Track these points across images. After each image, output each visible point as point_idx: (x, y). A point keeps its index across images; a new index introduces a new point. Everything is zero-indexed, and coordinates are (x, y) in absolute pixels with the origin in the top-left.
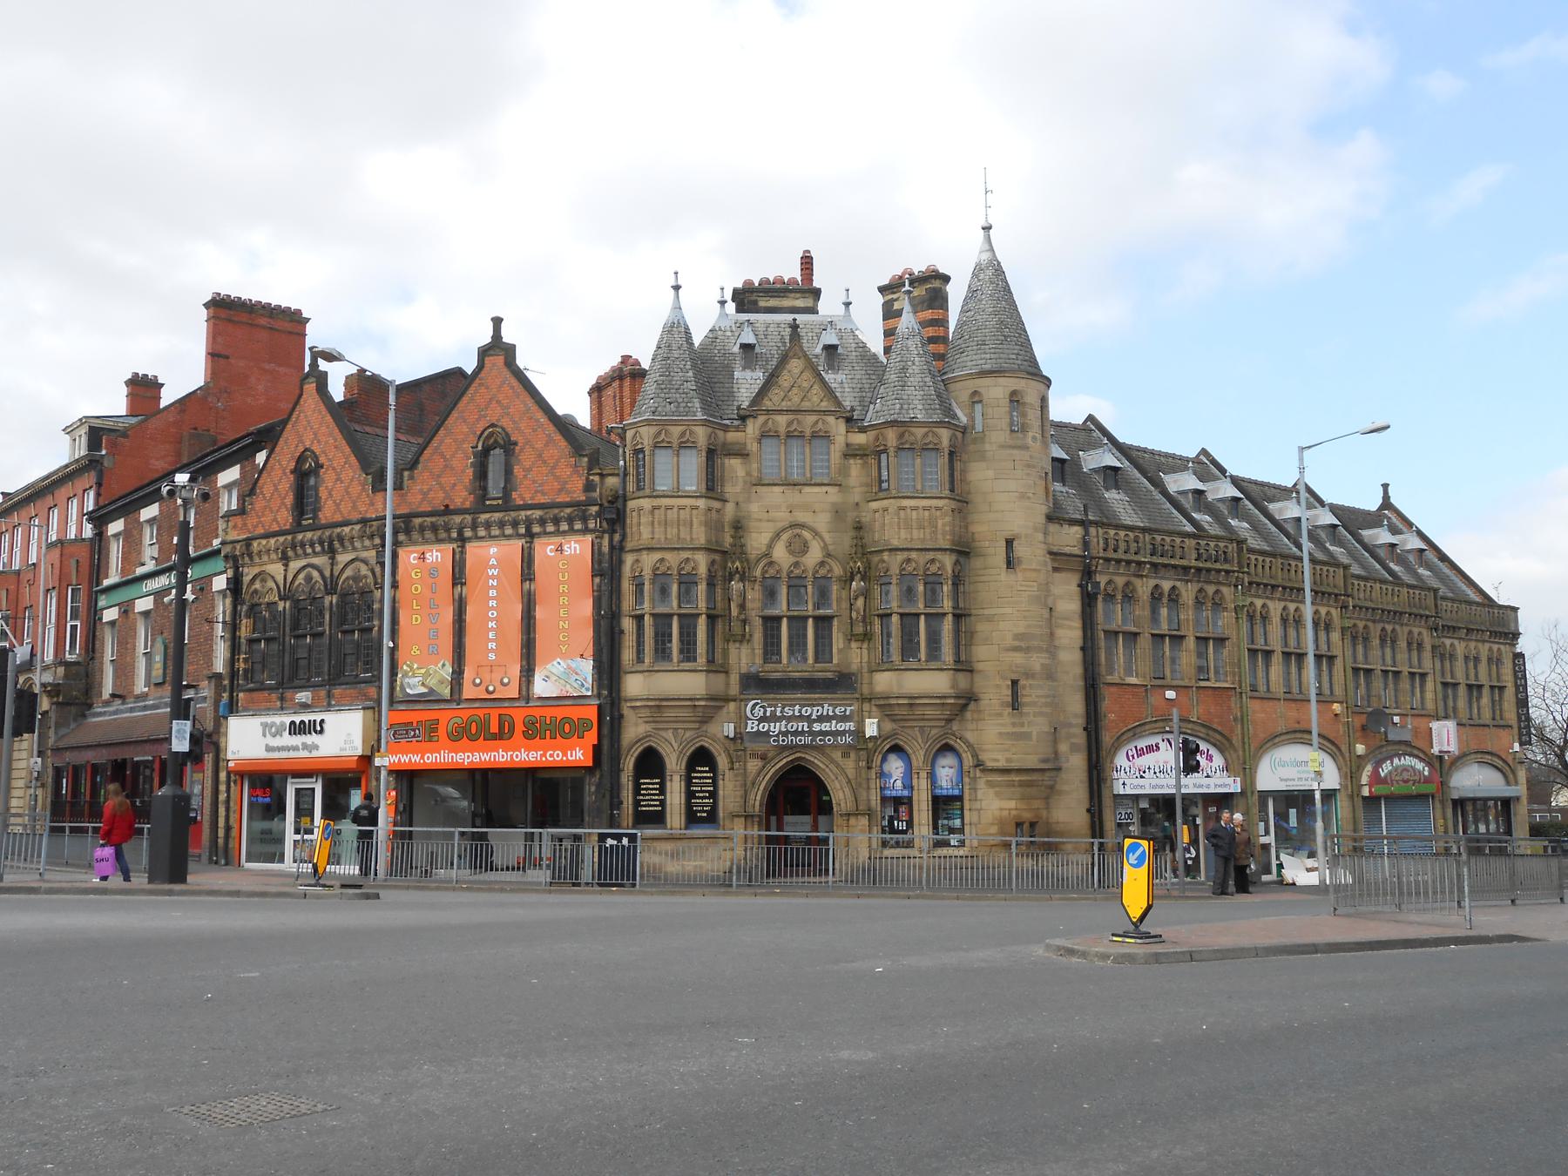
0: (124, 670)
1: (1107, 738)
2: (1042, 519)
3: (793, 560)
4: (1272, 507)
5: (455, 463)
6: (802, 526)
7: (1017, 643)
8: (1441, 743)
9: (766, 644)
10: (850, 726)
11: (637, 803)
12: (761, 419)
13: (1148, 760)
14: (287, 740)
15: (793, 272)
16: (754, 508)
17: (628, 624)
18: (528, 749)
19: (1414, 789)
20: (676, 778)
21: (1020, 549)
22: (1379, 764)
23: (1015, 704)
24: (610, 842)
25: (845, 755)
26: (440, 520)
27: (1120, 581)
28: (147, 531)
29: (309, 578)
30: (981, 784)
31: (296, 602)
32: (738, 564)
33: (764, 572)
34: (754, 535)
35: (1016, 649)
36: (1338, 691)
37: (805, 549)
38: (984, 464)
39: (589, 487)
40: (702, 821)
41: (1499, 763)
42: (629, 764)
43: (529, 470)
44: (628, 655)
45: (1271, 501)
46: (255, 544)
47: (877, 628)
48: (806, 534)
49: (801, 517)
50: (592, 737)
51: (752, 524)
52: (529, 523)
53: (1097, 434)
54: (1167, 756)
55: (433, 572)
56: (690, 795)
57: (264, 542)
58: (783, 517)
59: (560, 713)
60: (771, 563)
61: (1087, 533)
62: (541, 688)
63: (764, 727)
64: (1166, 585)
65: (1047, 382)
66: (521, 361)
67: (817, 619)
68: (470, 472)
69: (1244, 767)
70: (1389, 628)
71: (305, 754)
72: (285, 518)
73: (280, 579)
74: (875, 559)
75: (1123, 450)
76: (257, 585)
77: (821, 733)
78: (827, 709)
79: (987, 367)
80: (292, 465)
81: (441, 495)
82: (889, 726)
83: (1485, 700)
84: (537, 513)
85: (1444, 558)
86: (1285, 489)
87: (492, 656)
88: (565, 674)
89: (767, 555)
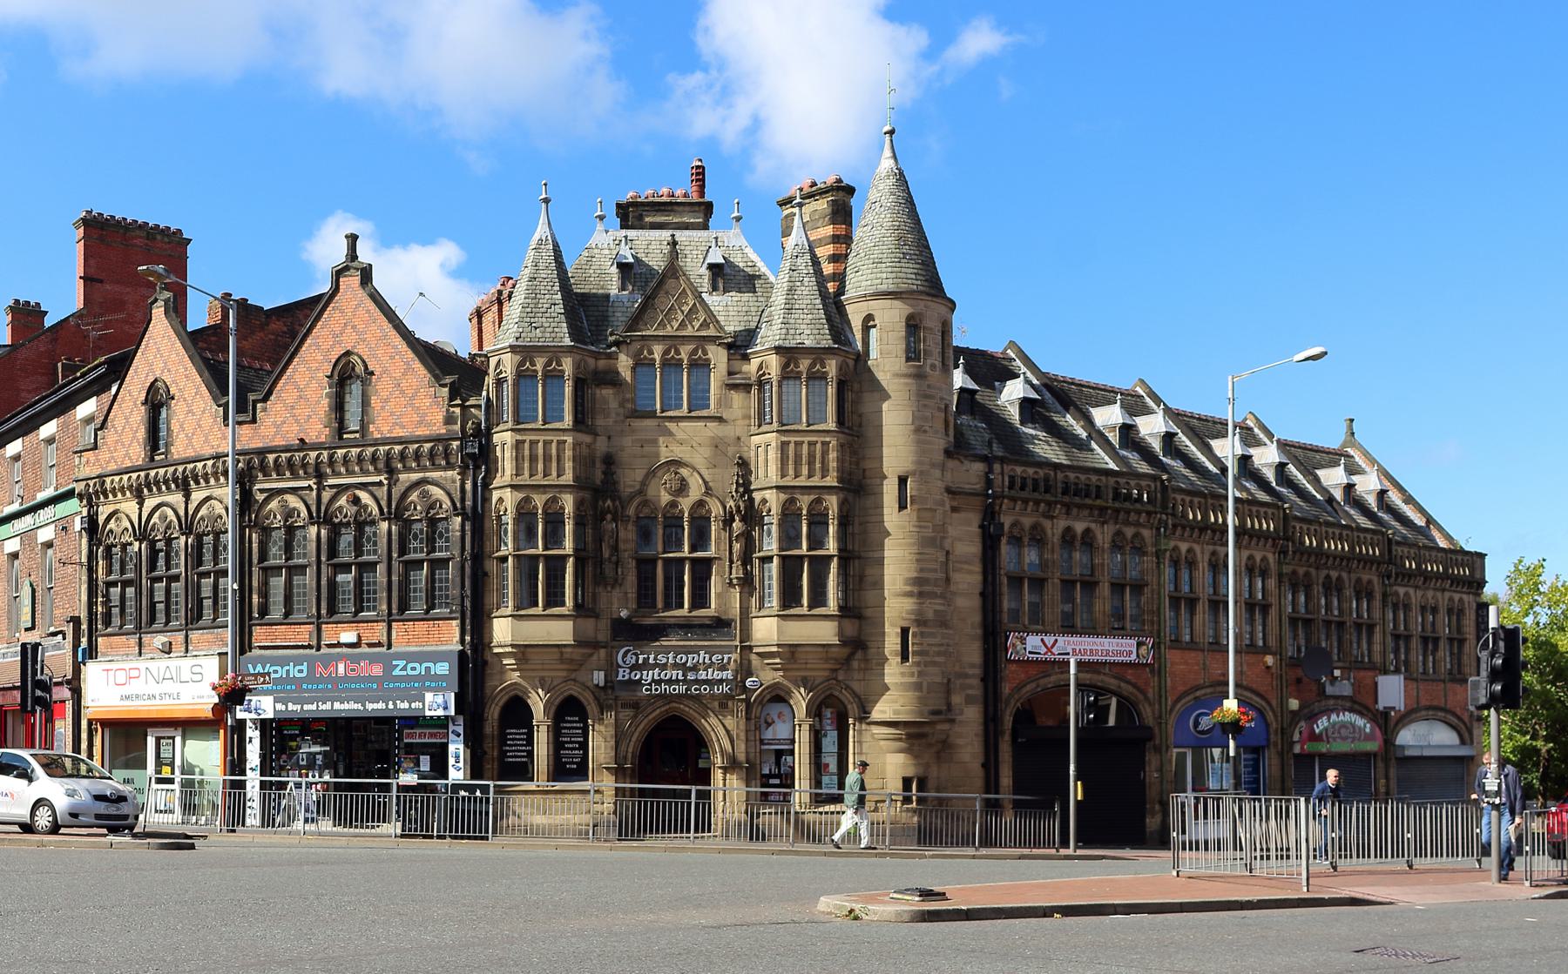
2: (939, 457)
7: (908, 588)
12: (637, 345)
15: (683, 188)
20: (543, 729)
26: (298, 456)
29: (164, 518)
30: (867, 737)
31: (152, 543)
39: (449, 420)
41: (1454, 720)
43: (386, 401)
48: (684, 472)
57: (117, 478)
60: (646, 503)
64: (1079, 527)
65: (952, 305)
67: (694, 561)
68: (325, 402)
72: (136, 453)
76: (112, 525)
79: (884, 288)
81: (295, 428)
89: (641, 492)
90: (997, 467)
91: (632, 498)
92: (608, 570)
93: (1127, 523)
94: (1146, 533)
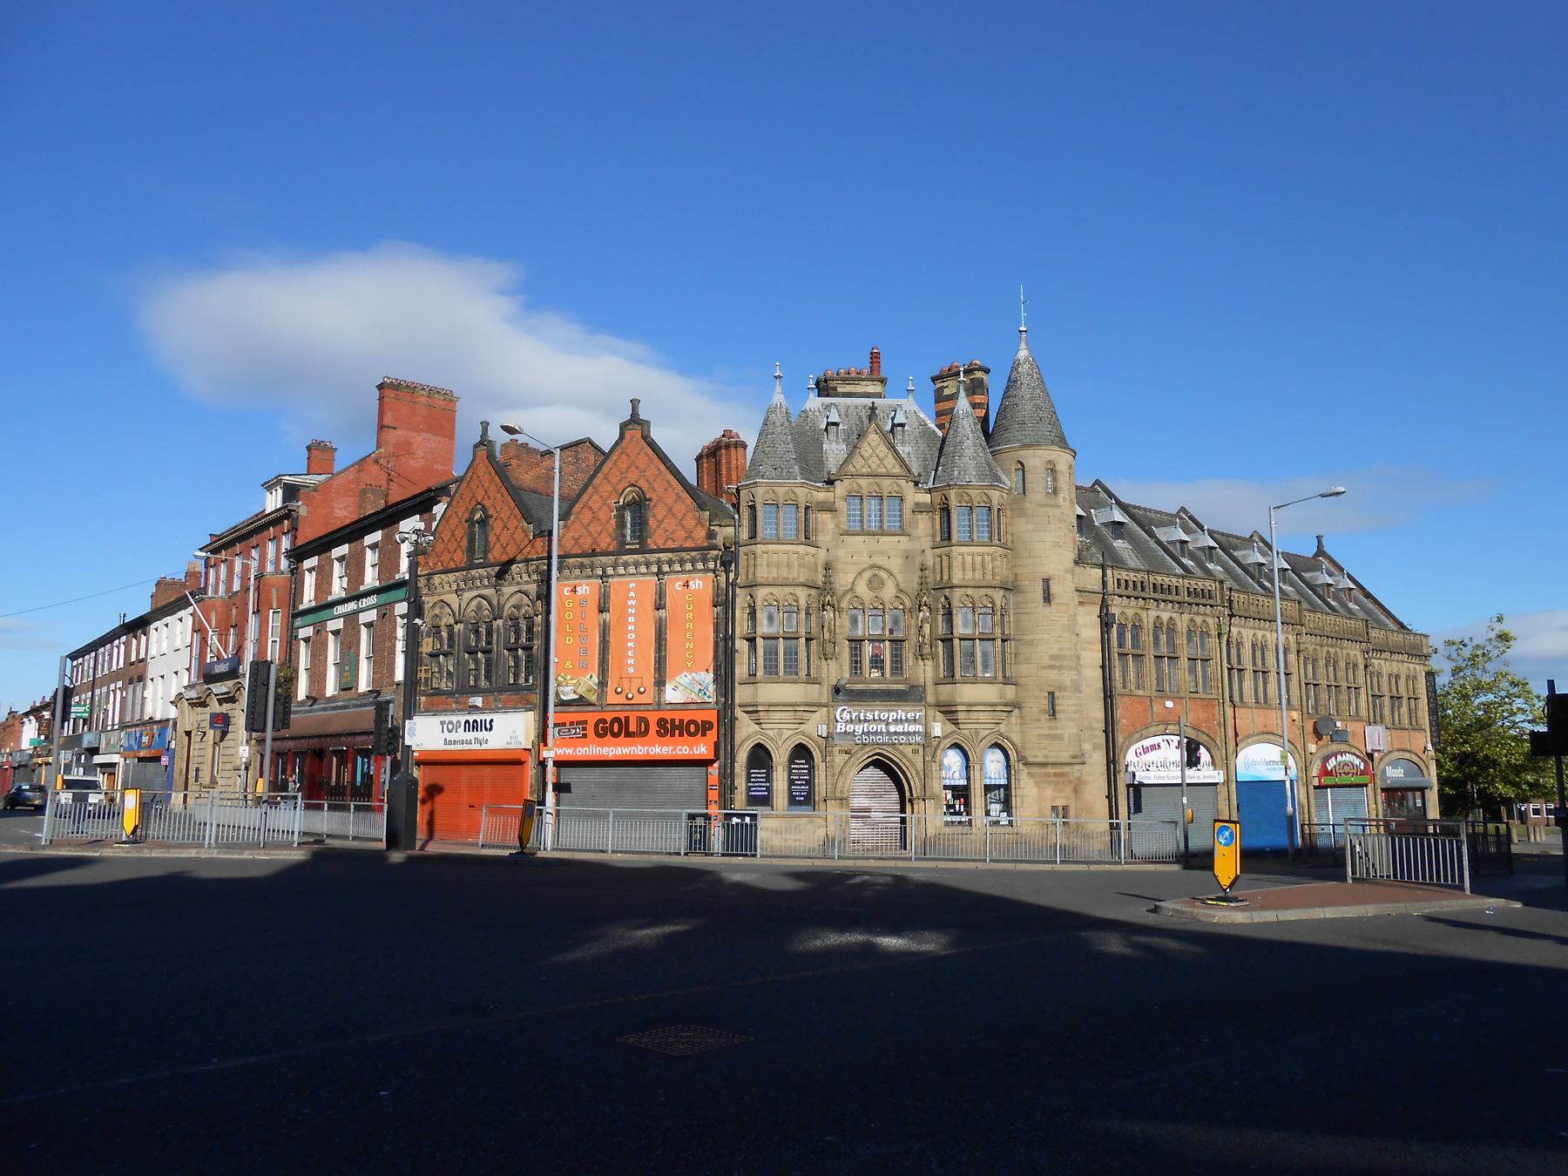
0: (317, 677)
1: (1120, 739)
2: (1070, 564)
4: (1158, 532)
5: (600, 515)
6: (880, 567)
8: (1372, 743)
10: (920, 728)
11: (749, 789)
13: (1151, 756)
14: (461, 734)
16: (842, 553)
17: (741, 645)
18: (662, 745)
19: (1353, 780)
20: (780, 769)
21: (1054, 589)
22: (1326, 759)
23: (1053, 712)
24: (735, 820)
25: (915, 752)
26: (585, 561)
27: (1130, 612)
28: (336, 565)
35: (1051, 667)
36: (1295, 701)
38: (1023, 520)
40: (800, 803)
42: (742, 757)
44: (741, 670)
45: (1235, 549)
46: (436, 577)
48: (883, 574)
49: (879, 560)
50: (712, 735)
51: (840, 566)
52: (659, 563)
53: (1103, 495)
54: (1171, 752)
55: (583, 601)
56: (791, 782)
58: (864, 560)
59: (687, 716)
61: (1104, 575)
62: (671, 695)
63: (850, 728)
64: (1165, 616)
66: (656, 434)
69: (1224, 762)
70: (1332, 651)
71: (477, 747)
72: (460, 557)
73: (455, 607)
75: (1124, 508)
77: (896, 733)
78: (901, 714)
80: (466, 516)
81: (590, 540)
82: (951, 728)
83: (1404, 709)
84: (664, 556)
85: (1368, 595)
86: (1244, 539)
87: (631, 670)
88: (689, 685)
89: (851, 590)
90: (1109, 572)
91: (845, 593)
93: (1197, 614)
94: (1210, 621)
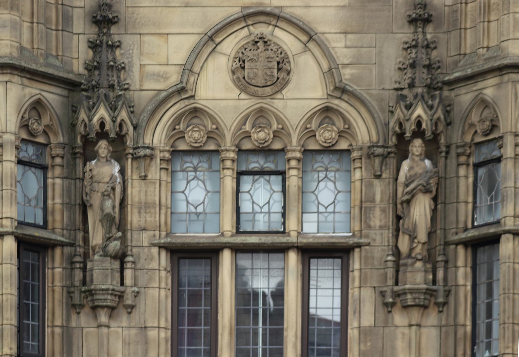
3: (247, 103)
6: (274, 17)
9: (177, 317)
32: (102, 112)
33: (176, 134)
34: (150, 42)
37: (281, 70)
47: (462, 275)
48: (286, 40)
74: (464, 97)
92: (102, 274)
